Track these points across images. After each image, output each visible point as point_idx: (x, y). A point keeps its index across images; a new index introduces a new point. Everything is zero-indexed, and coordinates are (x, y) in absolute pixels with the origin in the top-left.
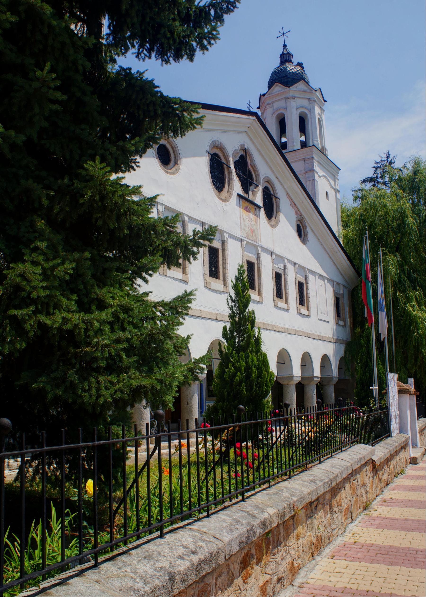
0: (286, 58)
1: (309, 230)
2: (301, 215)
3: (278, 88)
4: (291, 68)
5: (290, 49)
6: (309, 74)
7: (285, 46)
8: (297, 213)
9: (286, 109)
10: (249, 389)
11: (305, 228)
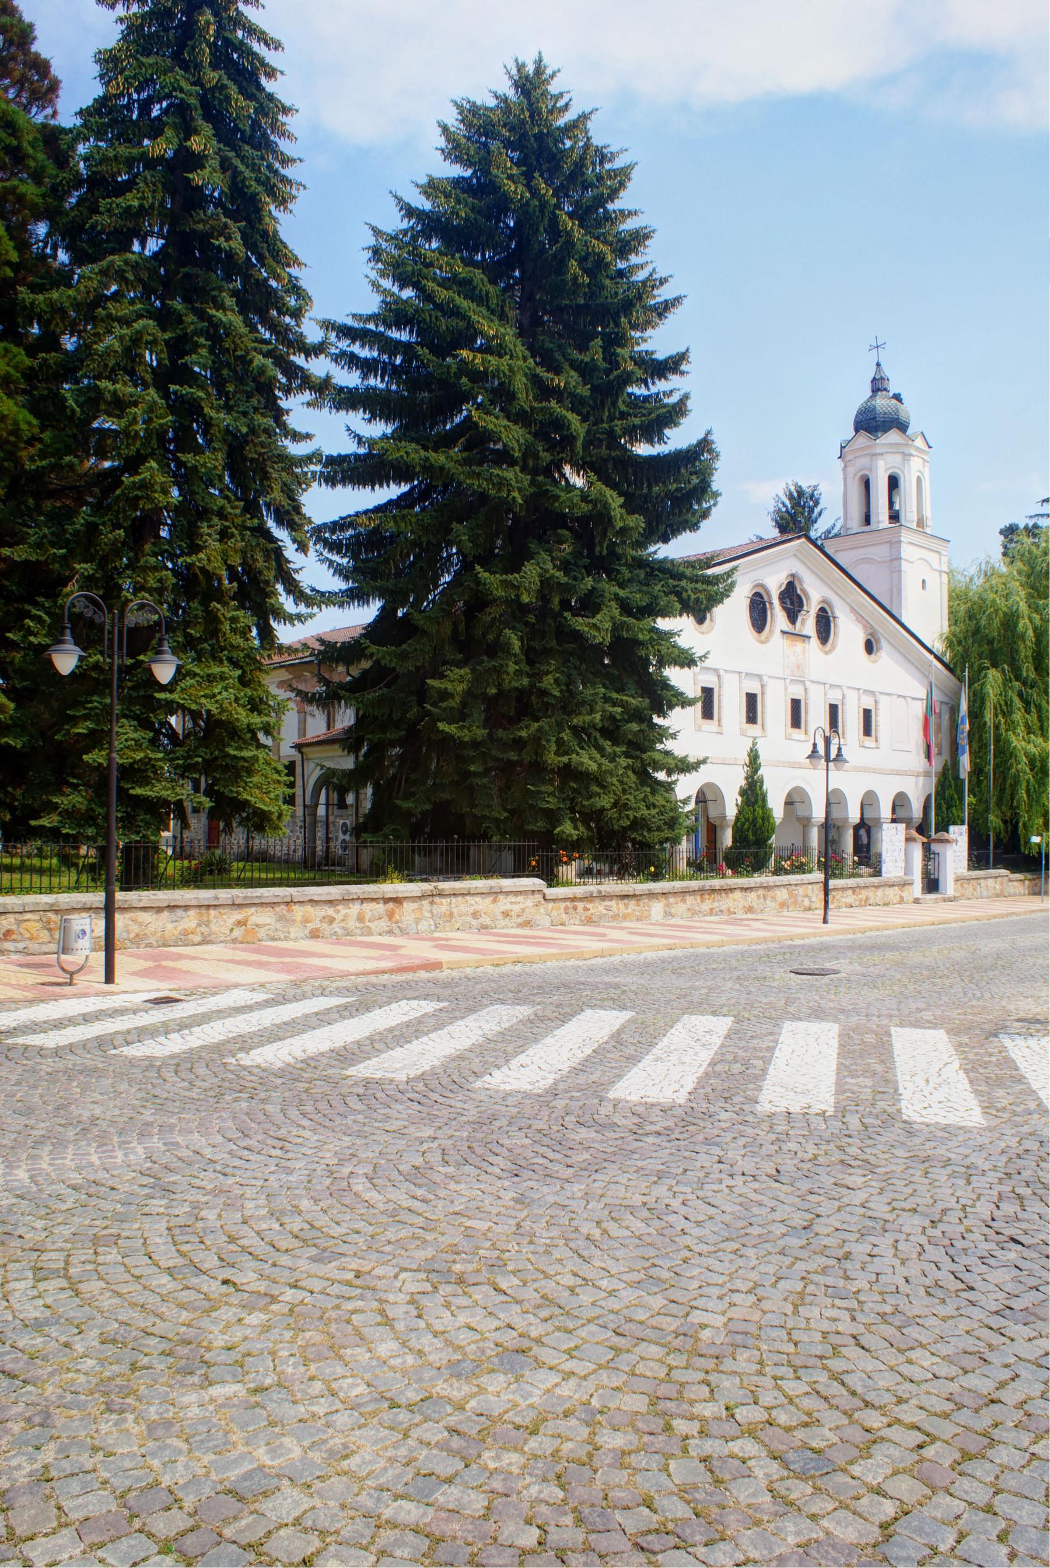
0: (878, 385)
1: (884, 643)
2: (872, 627)
3: (863, 439)
4: (882, 403)
5: (887, 371)
6: (911, 410)
7: (878, 365)
8: (865, 627)
9: (870, 470)
10: (755, 834)
11: (878, 641)
